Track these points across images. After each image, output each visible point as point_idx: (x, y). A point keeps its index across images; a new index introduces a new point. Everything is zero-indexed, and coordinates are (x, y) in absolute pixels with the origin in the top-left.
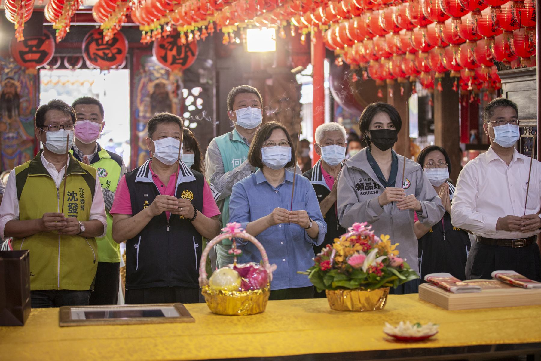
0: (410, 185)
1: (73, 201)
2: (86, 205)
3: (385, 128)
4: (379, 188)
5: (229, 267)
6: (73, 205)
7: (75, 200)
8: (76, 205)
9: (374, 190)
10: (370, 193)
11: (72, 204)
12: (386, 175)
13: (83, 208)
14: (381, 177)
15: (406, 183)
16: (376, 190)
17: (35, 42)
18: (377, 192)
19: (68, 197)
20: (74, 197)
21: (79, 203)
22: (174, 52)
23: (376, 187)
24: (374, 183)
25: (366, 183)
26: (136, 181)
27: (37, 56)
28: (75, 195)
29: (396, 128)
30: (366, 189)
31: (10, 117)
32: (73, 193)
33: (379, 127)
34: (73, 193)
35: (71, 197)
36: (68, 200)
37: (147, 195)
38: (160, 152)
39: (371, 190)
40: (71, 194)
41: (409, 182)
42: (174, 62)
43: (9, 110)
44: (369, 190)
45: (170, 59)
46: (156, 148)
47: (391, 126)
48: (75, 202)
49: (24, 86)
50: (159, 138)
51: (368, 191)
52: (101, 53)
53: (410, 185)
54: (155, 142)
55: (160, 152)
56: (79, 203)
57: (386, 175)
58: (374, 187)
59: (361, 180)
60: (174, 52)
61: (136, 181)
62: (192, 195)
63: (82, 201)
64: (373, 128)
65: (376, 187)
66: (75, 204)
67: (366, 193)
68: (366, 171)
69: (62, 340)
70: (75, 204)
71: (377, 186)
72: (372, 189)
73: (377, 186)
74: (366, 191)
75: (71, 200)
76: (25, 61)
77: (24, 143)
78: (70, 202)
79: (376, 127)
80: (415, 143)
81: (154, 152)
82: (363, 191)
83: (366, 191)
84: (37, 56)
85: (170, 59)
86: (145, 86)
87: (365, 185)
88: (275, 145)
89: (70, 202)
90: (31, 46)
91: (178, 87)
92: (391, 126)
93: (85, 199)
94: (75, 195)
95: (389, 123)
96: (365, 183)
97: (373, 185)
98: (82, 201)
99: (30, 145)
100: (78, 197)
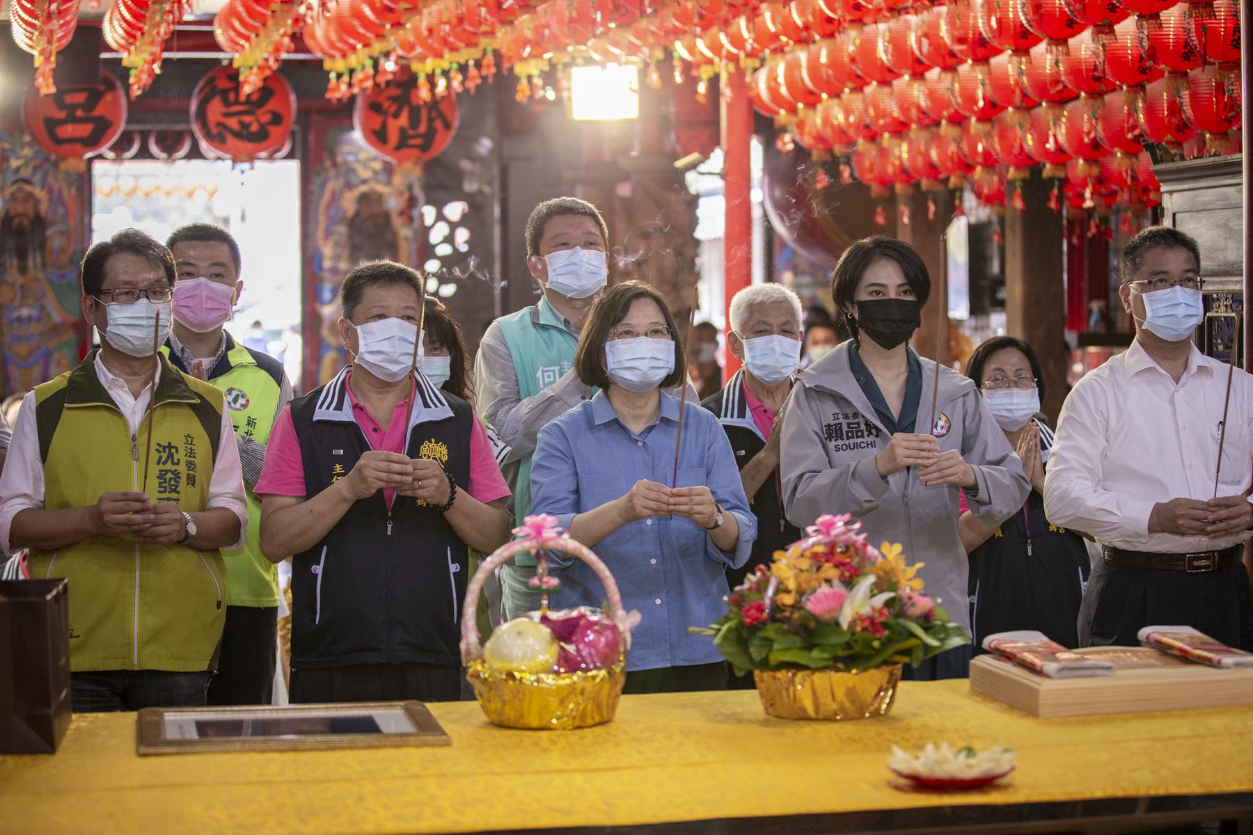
0: (949, 428)
1: (169, 466)
2: (199, 474)
3: (893, 295)
4: (877, 436)
5: (531, 618)
6: (170, 475)
7: (173, 463)
8: (177, 475)
9: (866, 439)
10: (857, 446)
11: (167, 471)
12: (894, 406)
13: (191, 480)
14: (883, 410)
15: (941, 423)
16: (872, 438)
17: (80, 98)
18: (873, 444)
19: (158, 455)
20: (171, 455)
21: (182, 469)
22: (403, 120)
23: (870, 434)
24: (867, 424)
25: (849, 424)
26: (315, 419)
27: (85, 130)
28: (173, 451)
29: (917, 296)
30: (848, 438)
31: (23, 270)
32: (170, 446)
33: (878, 293)
34: (170, 446)
35: (165, 456)
36: (158, 463)
37: (342, 452)
38: (371, 353)
39: (860, 440)
40: (164, 448)
41: (948, 421)
42: (402, 144)
43: (22, 255)
44: (855, 440)
45: (393, 136)
46: (361, 342)
47: (905, 292)
48: (173, 468)
49: (56, 199)
50: (367, 320)
51: (851, 441)
52: (233, 123)
53: (949, 428)
54: (359, 328)
55: (371, 353)
56: (182, 469)
57: (894, 406)
58: (866, 433)
59: (835, 415)
60: (403, 120)
61: (315, 419)
62: (446, 452)
63: (191, 465)
64: (863, 296)
65: (870, 434)
66: (173, 473)
67: (848, 447)
68: (847, 397)
69: (144, 787)
70: (173, 473)
71: (874, 431)
72: (863, 436)
73: (874, 431)
74: (847, 442)
75: (164, 463)
76: (58, 141)
77: (55, 330)
78: (162, 467)
79: (871, 293)
80: (961, 331)
81: (356, 352)
82: (840, 442)
83: (847, 442)
84: (85, 130)
85: (393, 136)
86: (335, 198)
87: (845, 428)
88: (638, 335)
89: (162, 467)
90: (73, 107)
91: (412, 202)
92: (905, 292)
93: (196, 461)
94: (173, 451)
95: (900, 286)
96: (844, 423)
97: (863, 427)
98: (191, 465)
99: (70, 336)
100: (181, 456)
